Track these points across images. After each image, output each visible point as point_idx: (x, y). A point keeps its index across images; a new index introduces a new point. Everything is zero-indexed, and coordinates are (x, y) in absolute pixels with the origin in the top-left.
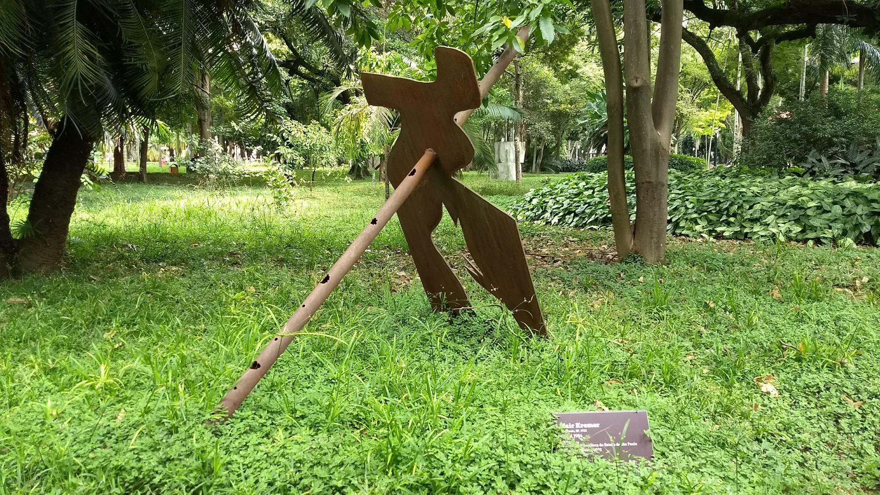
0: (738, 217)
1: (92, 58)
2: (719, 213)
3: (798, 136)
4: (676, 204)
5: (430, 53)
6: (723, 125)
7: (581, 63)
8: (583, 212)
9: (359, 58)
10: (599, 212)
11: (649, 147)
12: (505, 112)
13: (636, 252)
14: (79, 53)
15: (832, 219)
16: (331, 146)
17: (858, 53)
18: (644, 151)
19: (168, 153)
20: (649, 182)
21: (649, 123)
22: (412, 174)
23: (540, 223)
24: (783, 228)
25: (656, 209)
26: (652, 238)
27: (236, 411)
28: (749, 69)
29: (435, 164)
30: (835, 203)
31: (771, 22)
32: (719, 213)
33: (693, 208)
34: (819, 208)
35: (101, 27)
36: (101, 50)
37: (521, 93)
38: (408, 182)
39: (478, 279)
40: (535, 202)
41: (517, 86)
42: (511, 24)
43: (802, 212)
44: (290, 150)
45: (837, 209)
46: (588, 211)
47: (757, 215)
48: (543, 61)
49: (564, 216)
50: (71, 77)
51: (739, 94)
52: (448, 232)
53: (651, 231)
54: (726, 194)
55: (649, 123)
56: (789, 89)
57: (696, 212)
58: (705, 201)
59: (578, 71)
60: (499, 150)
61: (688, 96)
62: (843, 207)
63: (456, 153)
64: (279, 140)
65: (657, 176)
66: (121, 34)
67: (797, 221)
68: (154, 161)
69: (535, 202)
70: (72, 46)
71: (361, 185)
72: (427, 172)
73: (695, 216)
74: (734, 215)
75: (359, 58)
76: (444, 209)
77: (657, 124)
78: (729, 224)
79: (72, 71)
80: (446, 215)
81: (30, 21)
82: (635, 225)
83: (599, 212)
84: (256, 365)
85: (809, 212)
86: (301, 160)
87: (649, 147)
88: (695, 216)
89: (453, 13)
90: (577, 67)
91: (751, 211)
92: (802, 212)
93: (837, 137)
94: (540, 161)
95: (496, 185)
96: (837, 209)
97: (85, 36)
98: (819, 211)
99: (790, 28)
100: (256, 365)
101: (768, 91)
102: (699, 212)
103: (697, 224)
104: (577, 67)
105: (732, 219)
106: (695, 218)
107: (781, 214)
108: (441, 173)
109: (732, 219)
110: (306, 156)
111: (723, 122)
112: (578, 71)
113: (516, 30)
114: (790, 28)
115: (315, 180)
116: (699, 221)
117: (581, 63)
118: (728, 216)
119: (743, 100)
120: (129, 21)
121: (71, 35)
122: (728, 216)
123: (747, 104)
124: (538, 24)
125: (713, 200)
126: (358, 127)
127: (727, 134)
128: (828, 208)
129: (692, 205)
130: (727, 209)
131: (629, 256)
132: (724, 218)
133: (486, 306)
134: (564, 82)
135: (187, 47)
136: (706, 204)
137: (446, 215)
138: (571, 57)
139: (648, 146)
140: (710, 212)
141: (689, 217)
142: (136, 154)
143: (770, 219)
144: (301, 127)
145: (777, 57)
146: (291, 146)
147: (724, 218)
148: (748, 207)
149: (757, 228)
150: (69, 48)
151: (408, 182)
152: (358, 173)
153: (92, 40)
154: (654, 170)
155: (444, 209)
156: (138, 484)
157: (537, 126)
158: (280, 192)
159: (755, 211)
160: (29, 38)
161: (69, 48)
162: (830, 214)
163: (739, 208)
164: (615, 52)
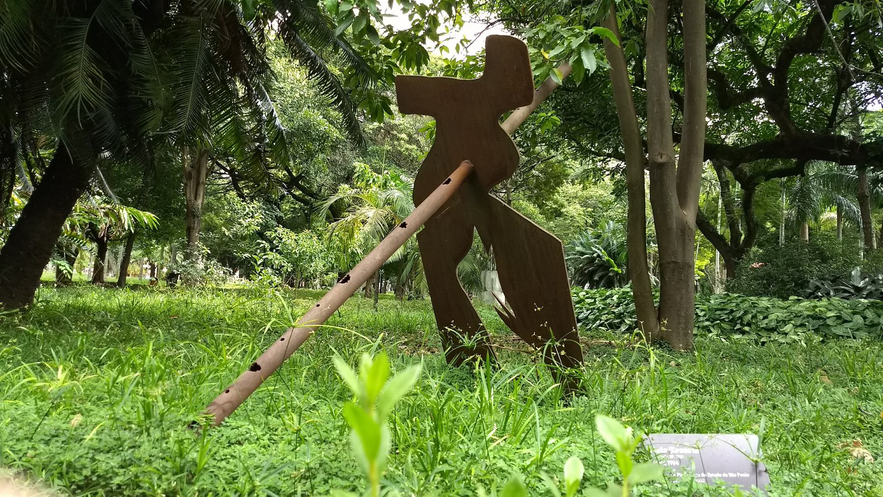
0: (753, 326)
1: (96, 82)
2: (733, 322)
3: (786, 277)
6: (703, 274)
7: (566, 203)
8: (587, 317)
9: (356, 175)
10: (604, 318)
11: (675, 225)
13: (662, 338)
14: (83, 80)
15: (855, 328)
16: (322, 255)
17: (835, 208)
18: (670, 229)
19: (149, 271)
20: (676, 263)
21: (674, 201)
22: (447, 183)
25: (684, 291)
26: (680, 323)
27: (227, 419)
28: (732, 215)
29: (470, 178)
30: (854, 313)
31: (761, 156)
33: (705, 316)
34: (838, 317)
35: (110, 53)
36: (106, 75)
38: (440, 193)
39: (509, 321)
43: (821, 322)
45: (858, 319)
46: (591, 317)
47: (773, 324)
48: (529, 199)
50: (71, 98)
51: (721, 238)
53: (679, 316)
54: (738, 305)
55: (674, 201)
56: (767, 241)
57: (707, 320)
58: (717, 310)
59: (563, 210)
60: (485, 278)
62: (865, 318)
63: (497, 161)
65: (684, 256)
66: (130, 65)
67: (817, 331)
68: (135, 275)
70: (77, 67)
73: (707, 323)
74: (749, 325)
75: (356, 175)
76: (476, 232)
78: (743, 333)
79: (73, 92)
80: (477, 241)
81: (35, 37)
82: (660, 308)
83: (604, 318)
84: (255, 368)
85: (829, 322)
87: (675, 225)
88: (707, 323)
90: (562, 206)
91: (766, 321)
92: (821, 322)
96: (858, 319)
97: (93, 59)
98: (839, 321)
99: (779, 165)
100: (255, 368)
101: (748, 242)
103: (710, 332)
104: (562, 206)
105: (747, 328)
106: (706, 326)
107: (798, 323)
108: (476, 187)
109: (747, 328)
110: (295, 263)
111: (702, 271)
112: (563, 210)
114: (779, 165)
116: (712, 329)
117: (566, 203)
118: (742, 325)
119: (726, 244)
120: (142, 56)
121: (78, 57)
123: (730, 247)
124: (579, 54)
125: (725, 309)
126: (351, 236)
127: (706, 284)
128: (849, 319)
129: (702, 314)
130: (740, 318)
132: (738, 326)
134: (549, 219)
135: (197, 86)
136: (718, 312)
137: (477, 241)
138: (556, 196)
141: (701, 324)
142: (116, 268)
143: (788, 328)
144: (293, 235)
145: (759, 205)
147: (738, 326)
148: (761, 317)
149: (775, 336)
150: (73, 69)
151: (440, 193)
153: (99, 63)
154: (680, 249)
155: (476, 232)
156: (87, 485)
159: (771, 320)
160: (30, 54)
161: (73, 69)
162: (851, 324)
163: (753, 317)
164: (636, 131)
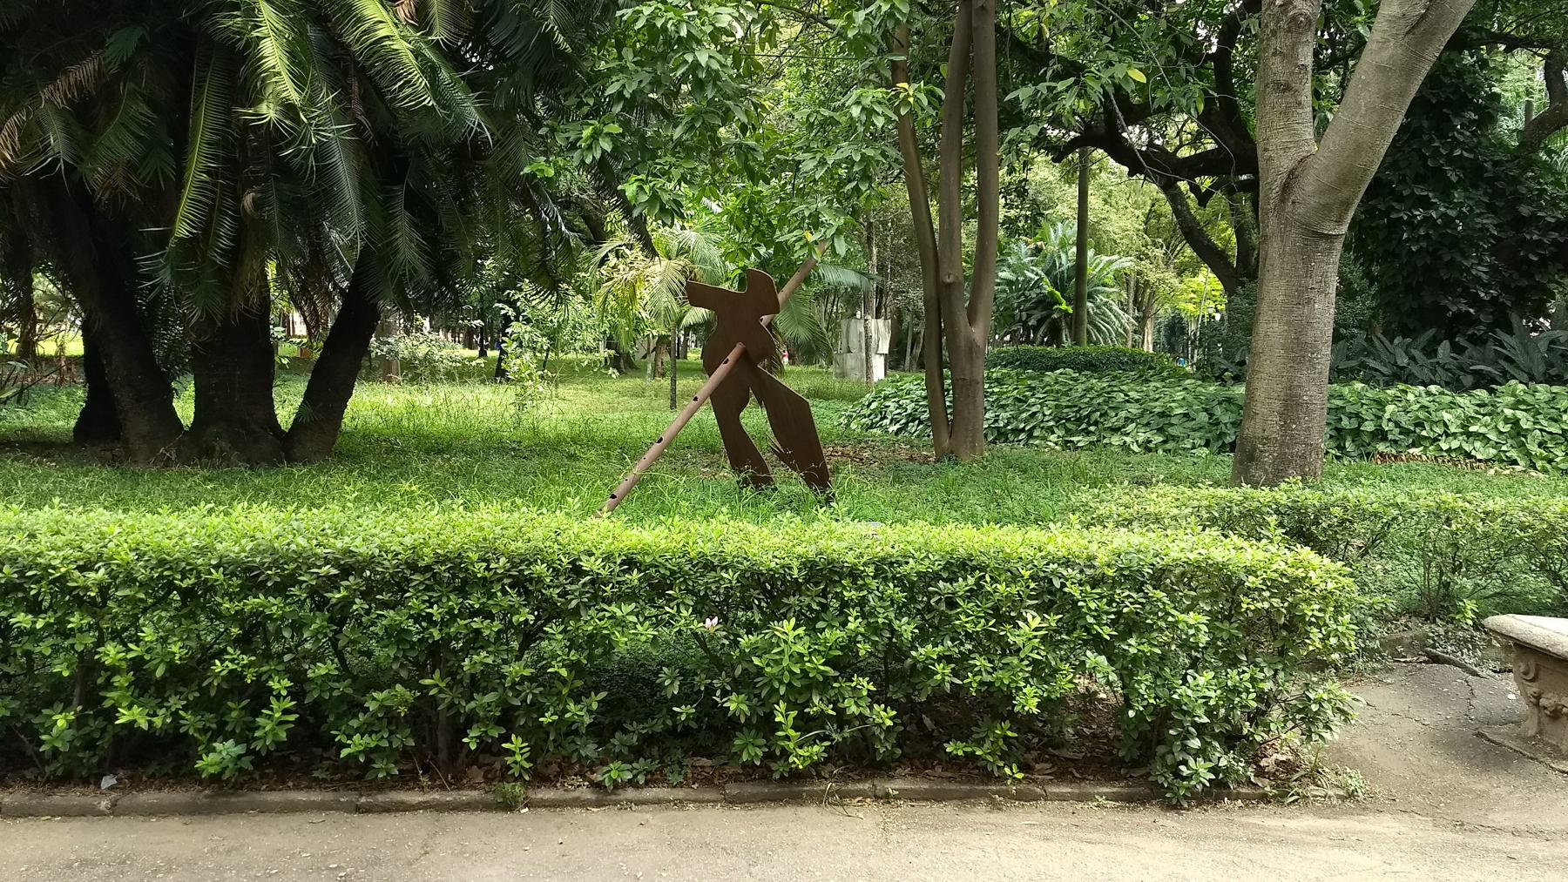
4: (1034, 409)
5: (740, 224)
12: (849, 278)
16: (590, 322)
23: (877, 431)
24: (1141, 437)
29: (744, 355)
32: (1079, 421)
37: (875, 250)
38: (722, 370)
39: (781, 457)
40: (873, 406)
41: (869, 240)
42: (811, 238)
44: (528, 328)
45: (1203, 417)
49: (906, 424)
52: (754, 418)
55: (962, 319)
61: (1159, 253)
64: (511, 313)
67: (1160, 430)
69: (873, 406)
71: (630, 383)
72: (737, 362)
74: (1096, 423)
77: (972, 321)
85: (1174, 421)
86: (544, 342)
89: (767, 182)
93: (1346, 327)
94: (918, 351)
95: (836, 384)
97: (414, 225)
100: (613, 497)
102: (1057, 419)
105: (1092, 428)
109: (1092, 428)
113: (816, 242)
115: (571, 373)
119: (1230, 265)
122: (1089, 424)
130: (1088, 416)
131: (948, 455)
133: (790, 483)
139: (962, 343)
140: (1068, 420)
146: (528, 321)
151: (722, 370)
152: (622, 363)
157: (911, 295)
158: (523, 387)
